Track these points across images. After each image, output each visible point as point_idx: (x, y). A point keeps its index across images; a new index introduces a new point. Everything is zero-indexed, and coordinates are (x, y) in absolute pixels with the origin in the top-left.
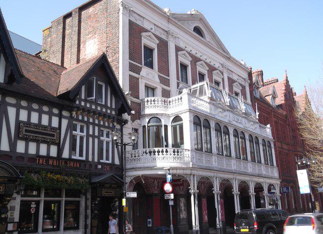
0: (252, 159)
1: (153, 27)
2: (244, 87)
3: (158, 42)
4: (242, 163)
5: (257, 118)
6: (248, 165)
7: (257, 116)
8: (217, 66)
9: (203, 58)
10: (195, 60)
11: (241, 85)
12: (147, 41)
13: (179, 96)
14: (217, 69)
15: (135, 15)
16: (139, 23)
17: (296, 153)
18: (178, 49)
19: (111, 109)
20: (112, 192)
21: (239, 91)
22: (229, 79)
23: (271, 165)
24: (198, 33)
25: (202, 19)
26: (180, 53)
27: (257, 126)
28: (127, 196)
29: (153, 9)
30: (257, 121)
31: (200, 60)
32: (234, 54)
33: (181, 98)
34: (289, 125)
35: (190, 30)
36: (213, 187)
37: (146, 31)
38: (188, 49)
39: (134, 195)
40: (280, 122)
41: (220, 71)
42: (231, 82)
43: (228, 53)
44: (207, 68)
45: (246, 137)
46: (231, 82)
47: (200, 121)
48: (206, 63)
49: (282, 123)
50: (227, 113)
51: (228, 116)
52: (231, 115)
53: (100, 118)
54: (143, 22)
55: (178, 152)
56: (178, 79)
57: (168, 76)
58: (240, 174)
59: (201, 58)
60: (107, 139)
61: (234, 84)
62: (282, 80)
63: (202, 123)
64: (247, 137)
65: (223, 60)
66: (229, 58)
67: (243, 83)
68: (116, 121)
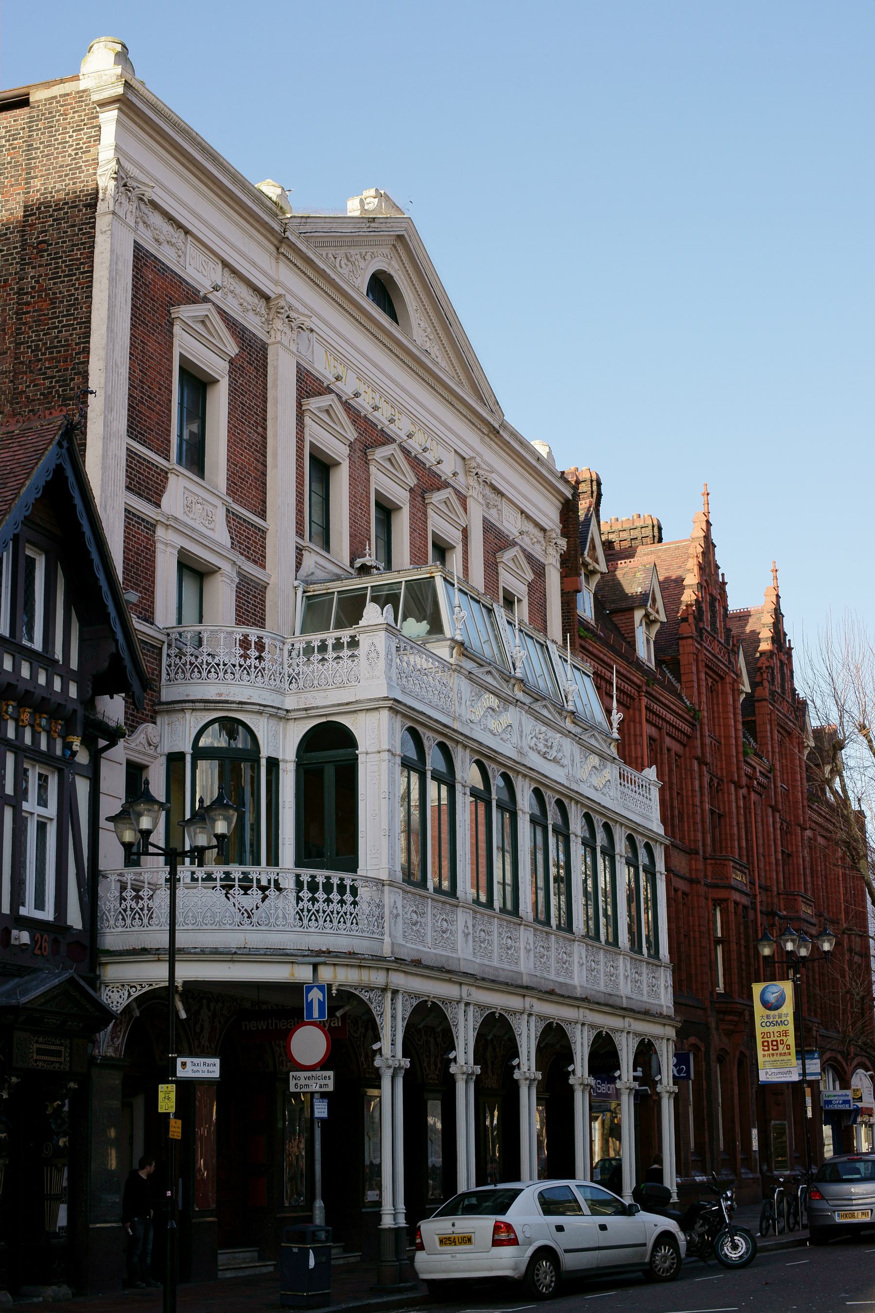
0: (632, 941)
1: (217, 275)
2: (539, 570)
3: (412, 481)
4: (431, 915)
5: (616, 735)
6: (570, 955)
7: (615, 725)
8: (448, 468)
9: (400, 428)
10: (370, 437)
11: (529, 557)
12: (198, 343)
13: (345, 635)
14: (206, 300)
15: (156, 219)
16: (167, 255)
17: (722, 894)
18: (309, 386)
19: (67, 676)
20: (58, 1054)
21: (520, 590)
22: (489, 528)
23: (649, 955)
24: (389, 320)
25: (404, 242)
26: (314, 404)
27: (611, 772)
28: (181, 1073)
29: (534, 468)
30: (613, 751)
31: (385, 439)
32: (516, 415)
33: (354, 643)
34: (702, 762)
35: (354, 287)
36: (453, 1048)
37: (193, 297)
38: (347, 387)
39: (203, 1068)
40: (668, 741)
41: (457, 492)
42: (496, 541)
43: (495, 408)
44: (352, 434)
45: (617, 850)
46: (496, 541)
47: (427, 748)
48: (406, 452)
49: (676, 747)
50: (512, 715)
51: (516, 726)
52: (529, 724)
53: (26, 717)
54: (181, 254)
55: (342, 889)
56: (300, 533)
57: (263, 515)
58: (550, 994)
59: (392, 429)
60: (41, 810)
61: (380, 453)
62: (682, 532)
63: (550, 817)
64: (525, 801)
65: (472, 441)
66: (496, 432)
67: (537, 551)
68: (79, 729)
